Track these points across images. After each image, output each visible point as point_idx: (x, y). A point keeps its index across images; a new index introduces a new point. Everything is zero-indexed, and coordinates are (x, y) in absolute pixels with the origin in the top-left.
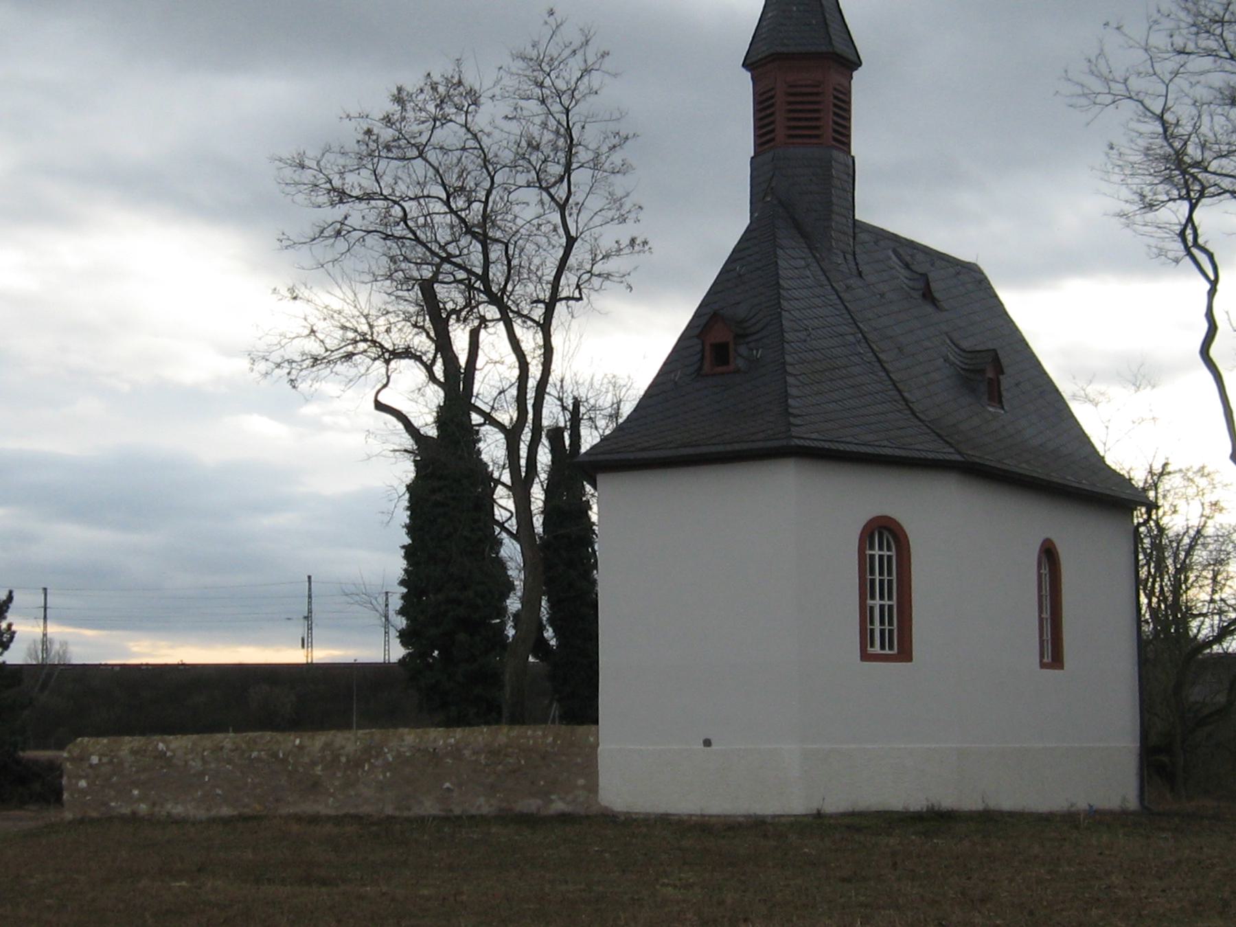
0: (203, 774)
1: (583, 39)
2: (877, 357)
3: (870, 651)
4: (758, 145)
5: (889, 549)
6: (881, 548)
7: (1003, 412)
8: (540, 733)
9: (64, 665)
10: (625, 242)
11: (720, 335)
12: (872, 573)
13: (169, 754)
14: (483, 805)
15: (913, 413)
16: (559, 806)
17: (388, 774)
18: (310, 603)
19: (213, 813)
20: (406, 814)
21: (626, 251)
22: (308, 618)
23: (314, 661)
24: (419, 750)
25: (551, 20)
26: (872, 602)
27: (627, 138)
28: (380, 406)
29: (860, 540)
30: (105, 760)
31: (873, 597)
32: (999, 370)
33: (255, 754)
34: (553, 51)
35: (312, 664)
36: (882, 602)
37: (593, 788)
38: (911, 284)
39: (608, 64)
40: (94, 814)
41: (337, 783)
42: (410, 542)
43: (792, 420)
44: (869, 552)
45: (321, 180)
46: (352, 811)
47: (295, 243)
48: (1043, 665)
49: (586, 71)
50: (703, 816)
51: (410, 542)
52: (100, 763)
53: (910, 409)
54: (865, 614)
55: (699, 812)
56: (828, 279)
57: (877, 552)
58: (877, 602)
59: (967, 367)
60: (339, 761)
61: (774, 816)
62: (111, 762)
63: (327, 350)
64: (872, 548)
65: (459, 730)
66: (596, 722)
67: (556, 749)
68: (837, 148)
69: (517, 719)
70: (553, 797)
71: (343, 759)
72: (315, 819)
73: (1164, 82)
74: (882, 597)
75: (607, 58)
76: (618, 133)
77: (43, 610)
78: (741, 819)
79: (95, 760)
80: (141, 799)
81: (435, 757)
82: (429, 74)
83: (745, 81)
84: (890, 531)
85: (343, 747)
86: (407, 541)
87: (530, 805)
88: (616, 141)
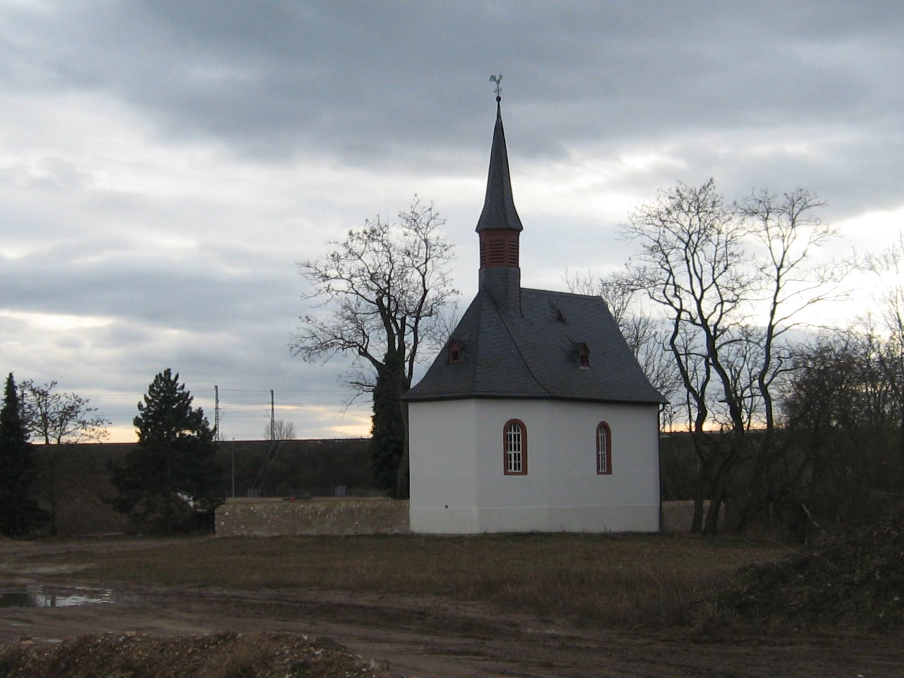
0: (268, 519)
3: (509, 471)
4: (481, 264)
6: (515, 431)
7: (588, 368)
11: (455, 348)
12: (511, 440)
14: (370, 531)
16: (396, 531)
25: (416, 198)
26: (510, 452)
29: (505, 428)
31: (511, 450)
32: (587, 350)
33: (287, 511)
37: (408, 524)
38: (552, 315)
47: (308, 297)
52: (229, 515)
54: (507, 457)
57: (513, 433)
58: (513, 452)
62: (233, 515)
64: (511, 431)
68: (511, 266)
71: (319, 513)
74: (515, 450)
79: (227, 514)
80: (245, 529)
81: (352, 512)
82: (367, 220)
83: (477, 236)
85: (319, 509)
86: (373, 414)
87: (387, 530)
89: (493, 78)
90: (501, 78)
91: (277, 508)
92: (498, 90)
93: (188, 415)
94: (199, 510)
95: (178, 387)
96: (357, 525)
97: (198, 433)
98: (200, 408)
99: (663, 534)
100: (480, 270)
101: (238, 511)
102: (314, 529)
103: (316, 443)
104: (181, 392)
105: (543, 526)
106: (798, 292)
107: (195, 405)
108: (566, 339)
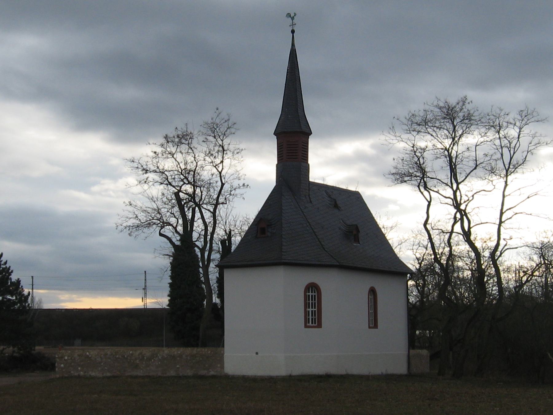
1: (228, 118)
2: (313, 231)
3: (308, 324)
5: (315, 293)
6: (312, 292)
7: (359, 245)
8: (206, 350)
9: (40, 309)
10: (241, 185)
12: (309, 300)
13: (90, 356)
14: (189, 373)
15: (324, 249)
16: (212, 373)
17: (159, 363)
18: (145, 283)
19: (105, 375)
20: (165, 375)
21: (242, 187)
22: (145, 289)
23: (147, 308)
24: (169, 355)
26: (309, 309)
27: (242, 150)
28: (161, 235)
30: (69, 358)
31: (309, 308)
32: (358, 231)
33: (117, 356)
34: (218, 121)
35: (146, 309)
36: (312, 309)
37: (222, 367)
39: (235, 126)
40: (66, 375)
41: (143, 366)
42: (171, 281)
43: (283, 253)
44: (308, 294)
45: (140, 166)
46: (147, 374)
47: (131, 186)
48: (370, 327)
49: (228, 128)
50: (255, 376)
51: (171, 281)
53: (323, 247)
54: (306, 313)
55: (254, 375)
56: (299, 205)
57: (310, 294)
58: (310, 310)
59: (347, 230)
60: (144, 359)
61: (277, 376)
62: (71, 359)
63: (141, 223)
65: (182, 348)
66: (223, 346)
67: (211, 355)
68: (304, 162)
69: (204, 345)
70: (210, 370)
71: (145, 358)
72: (136, 377)
73: (414, 136)
74: (312, 308)
75: (235, 125)
76: (239, 149)
77: (31, 286)
78: (266, 377)
79: (66, 358)
80: (81, 371)
82: (176, 128)
84: (315, 287)
85: (145, 354)
86: (170, 281)
87: (203, 372)
88: (238, 151)
89: (289, 15)
90: (295, 15)
91: (109, 353)
92: (293, 25)
93: (9, 284)
94: (15, 354)
95: (2, 263)
96: (178, 368)
97: (16, 297)
98: (18, 279)
99: (410, 376)
100: (277, 165)
101: (76, 356)
102: (141, 371)
103: (61, 311)
104: (4, 266)
105: (334, 370)
106: (519, 189)
107: (14, 277)
108: (341, 221)
